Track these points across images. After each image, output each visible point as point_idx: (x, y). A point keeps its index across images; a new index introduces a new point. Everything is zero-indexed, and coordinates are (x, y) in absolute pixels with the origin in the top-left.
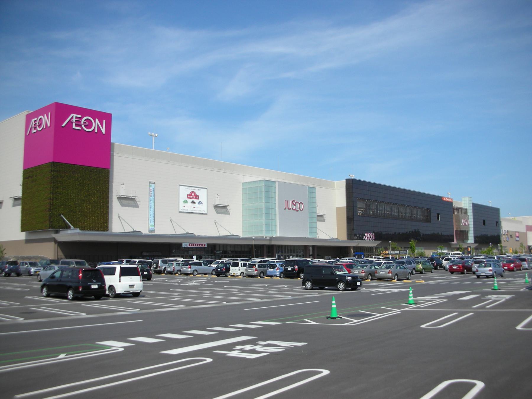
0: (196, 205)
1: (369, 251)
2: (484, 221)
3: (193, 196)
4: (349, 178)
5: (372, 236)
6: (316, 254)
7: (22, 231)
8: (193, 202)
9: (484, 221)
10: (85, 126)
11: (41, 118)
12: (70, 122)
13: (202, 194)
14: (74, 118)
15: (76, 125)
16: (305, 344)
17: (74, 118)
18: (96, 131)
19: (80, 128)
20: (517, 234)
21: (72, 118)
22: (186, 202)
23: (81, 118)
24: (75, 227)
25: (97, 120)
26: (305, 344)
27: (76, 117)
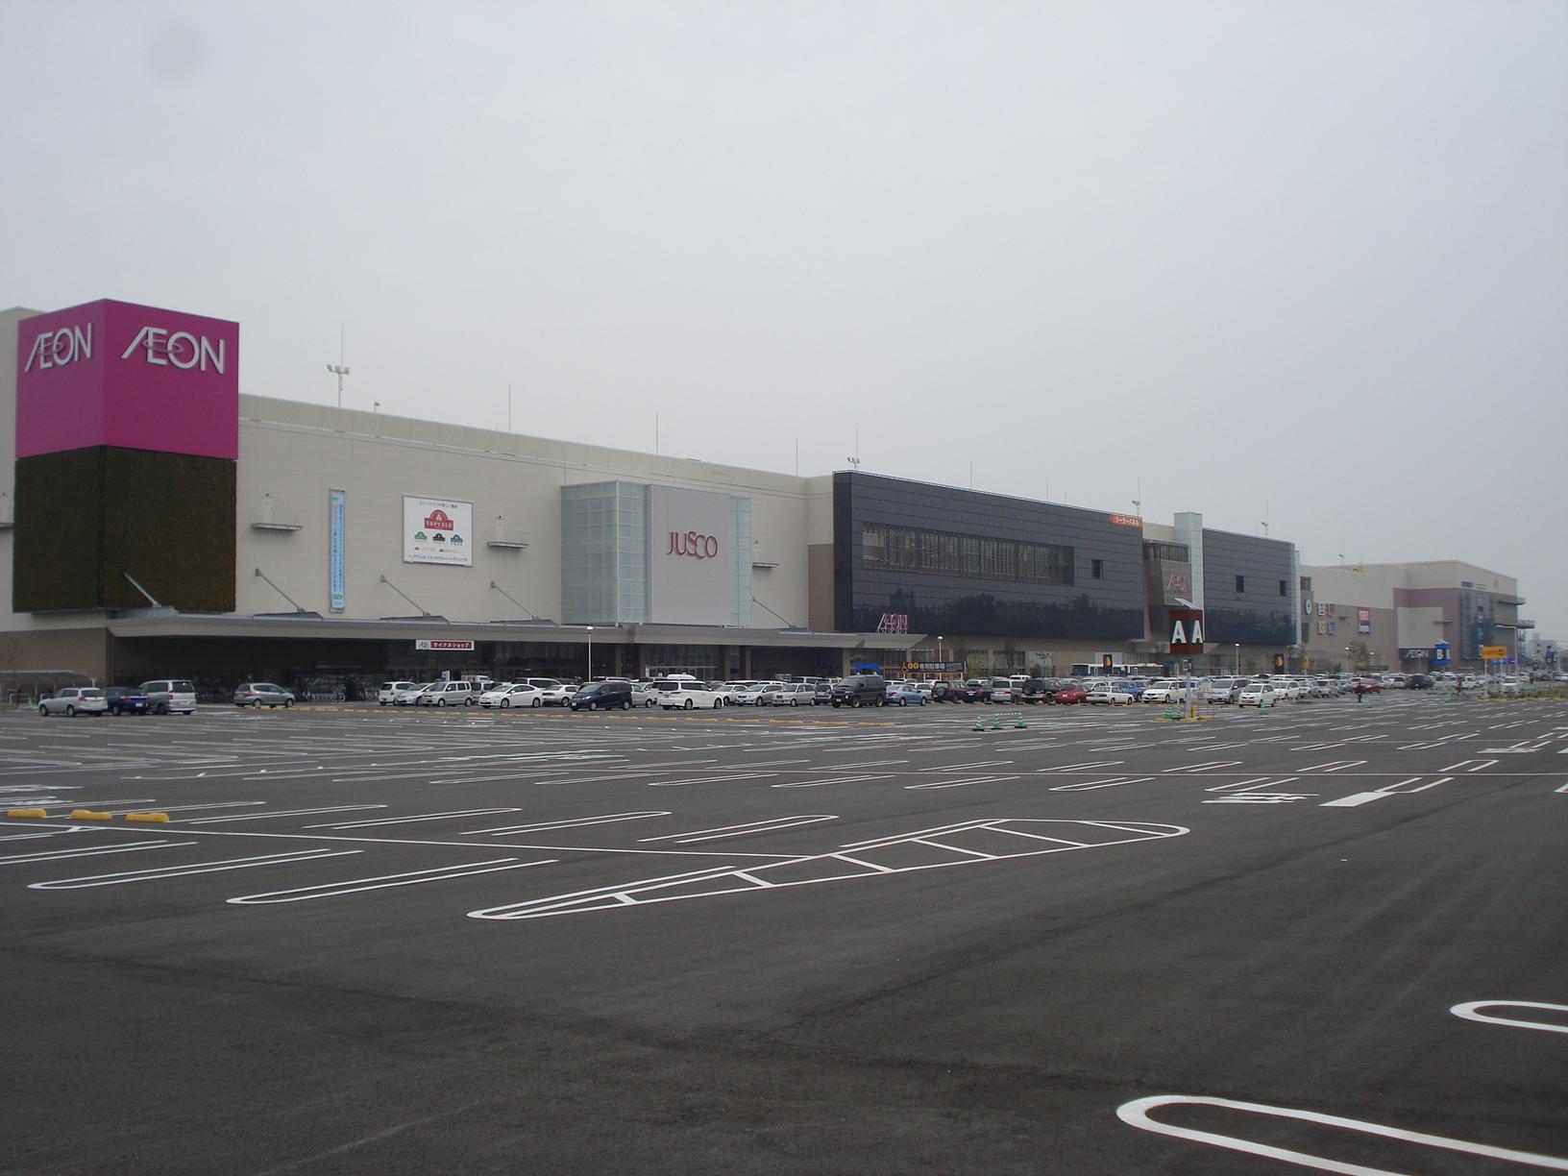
0: (447, 544)
1: (891, 662)
2: (1240, 580)
3: (439, 521)
4: (10, 607)
5: (903, 620)
6: (748, 668)
8: (439, 538)
9: (1240, 580)
10: (177, 355)
11: (64, 336)
12: (142, 348)
13: (461, 516)
15: (157, 354)
18: (203, 368)
19: (163, 362)
20: (1364, 615)
21: (146, 336)
22: (420, 536)
23: (167, 338)
24: (165, 603)
25: (204, 340)
27: (156, 336)
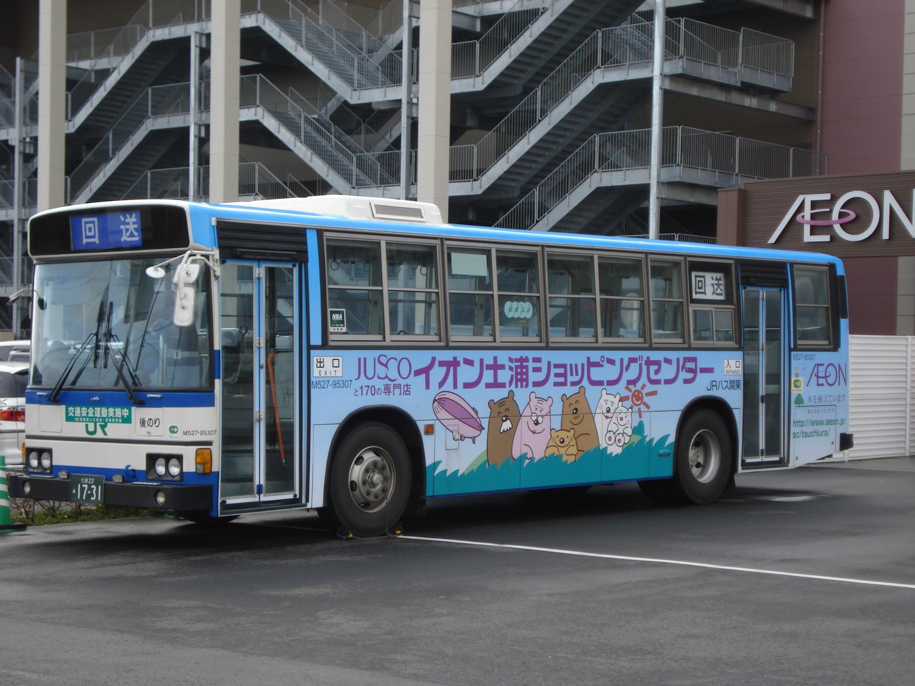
7: (742, 83)
14: (808, 206)
16: (257, 63)
17: (808, 206)
21: (801, 208)
25: (889, 198)
26: (257, 63)
27: (814, 204)
